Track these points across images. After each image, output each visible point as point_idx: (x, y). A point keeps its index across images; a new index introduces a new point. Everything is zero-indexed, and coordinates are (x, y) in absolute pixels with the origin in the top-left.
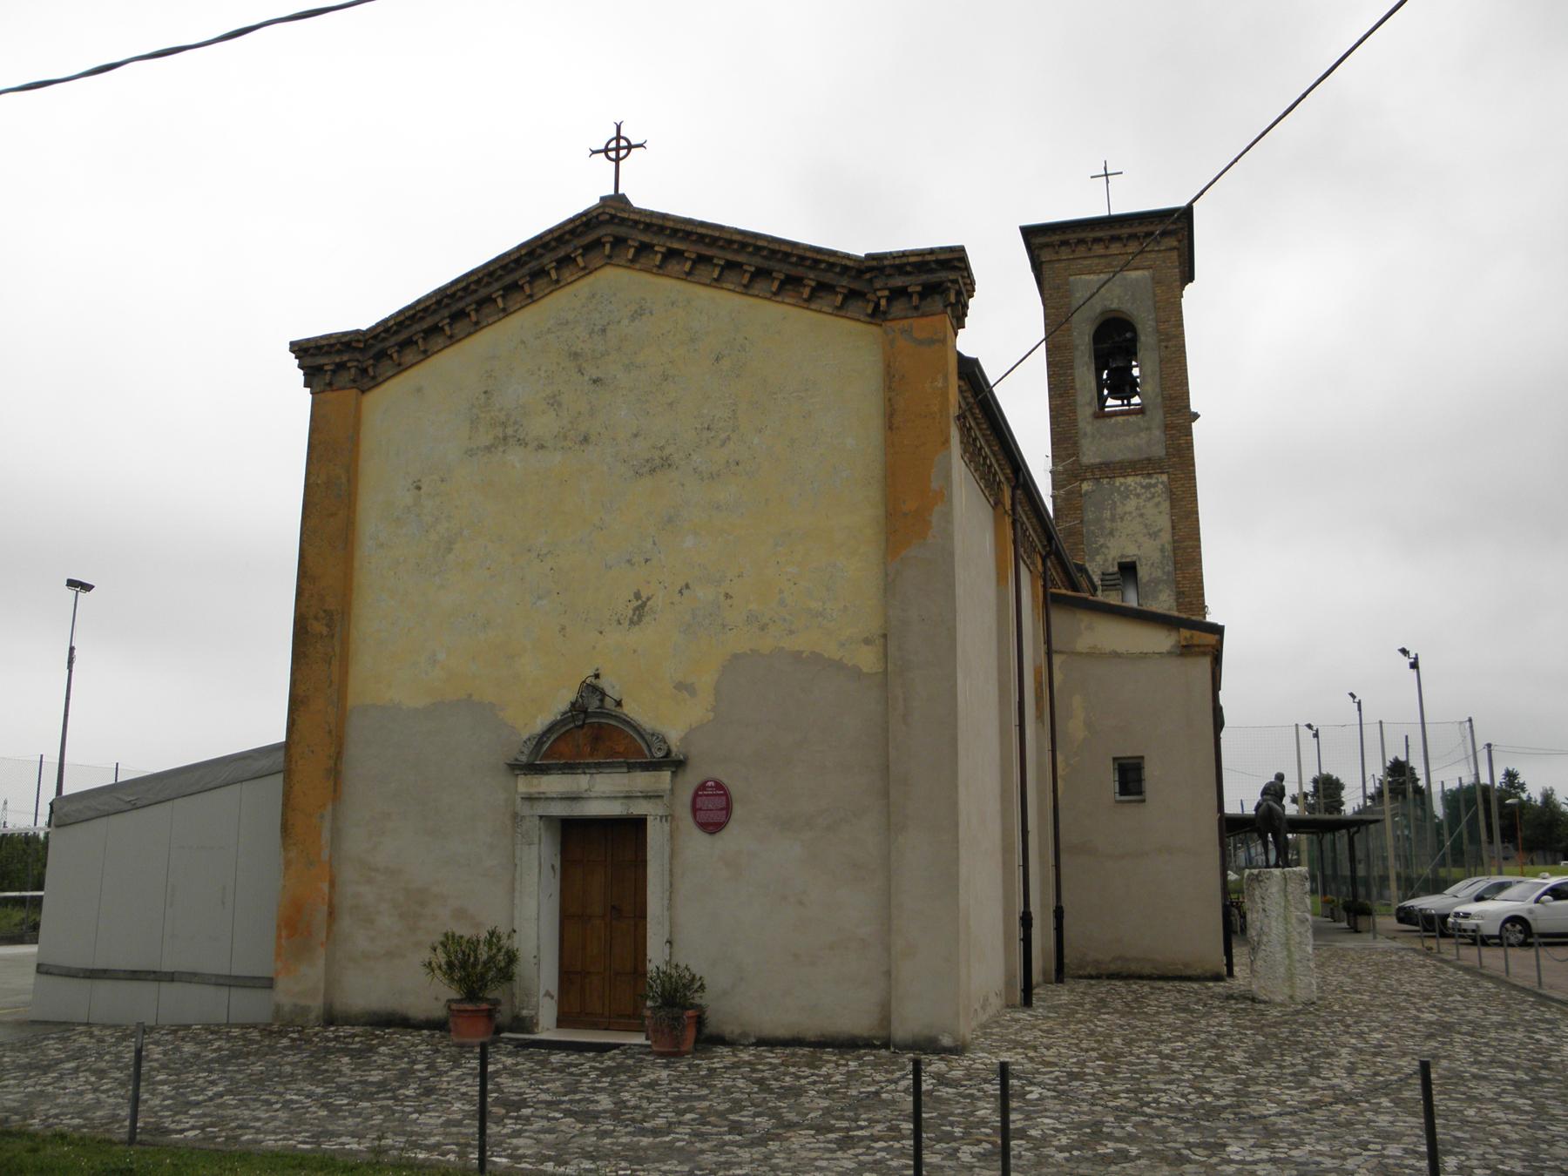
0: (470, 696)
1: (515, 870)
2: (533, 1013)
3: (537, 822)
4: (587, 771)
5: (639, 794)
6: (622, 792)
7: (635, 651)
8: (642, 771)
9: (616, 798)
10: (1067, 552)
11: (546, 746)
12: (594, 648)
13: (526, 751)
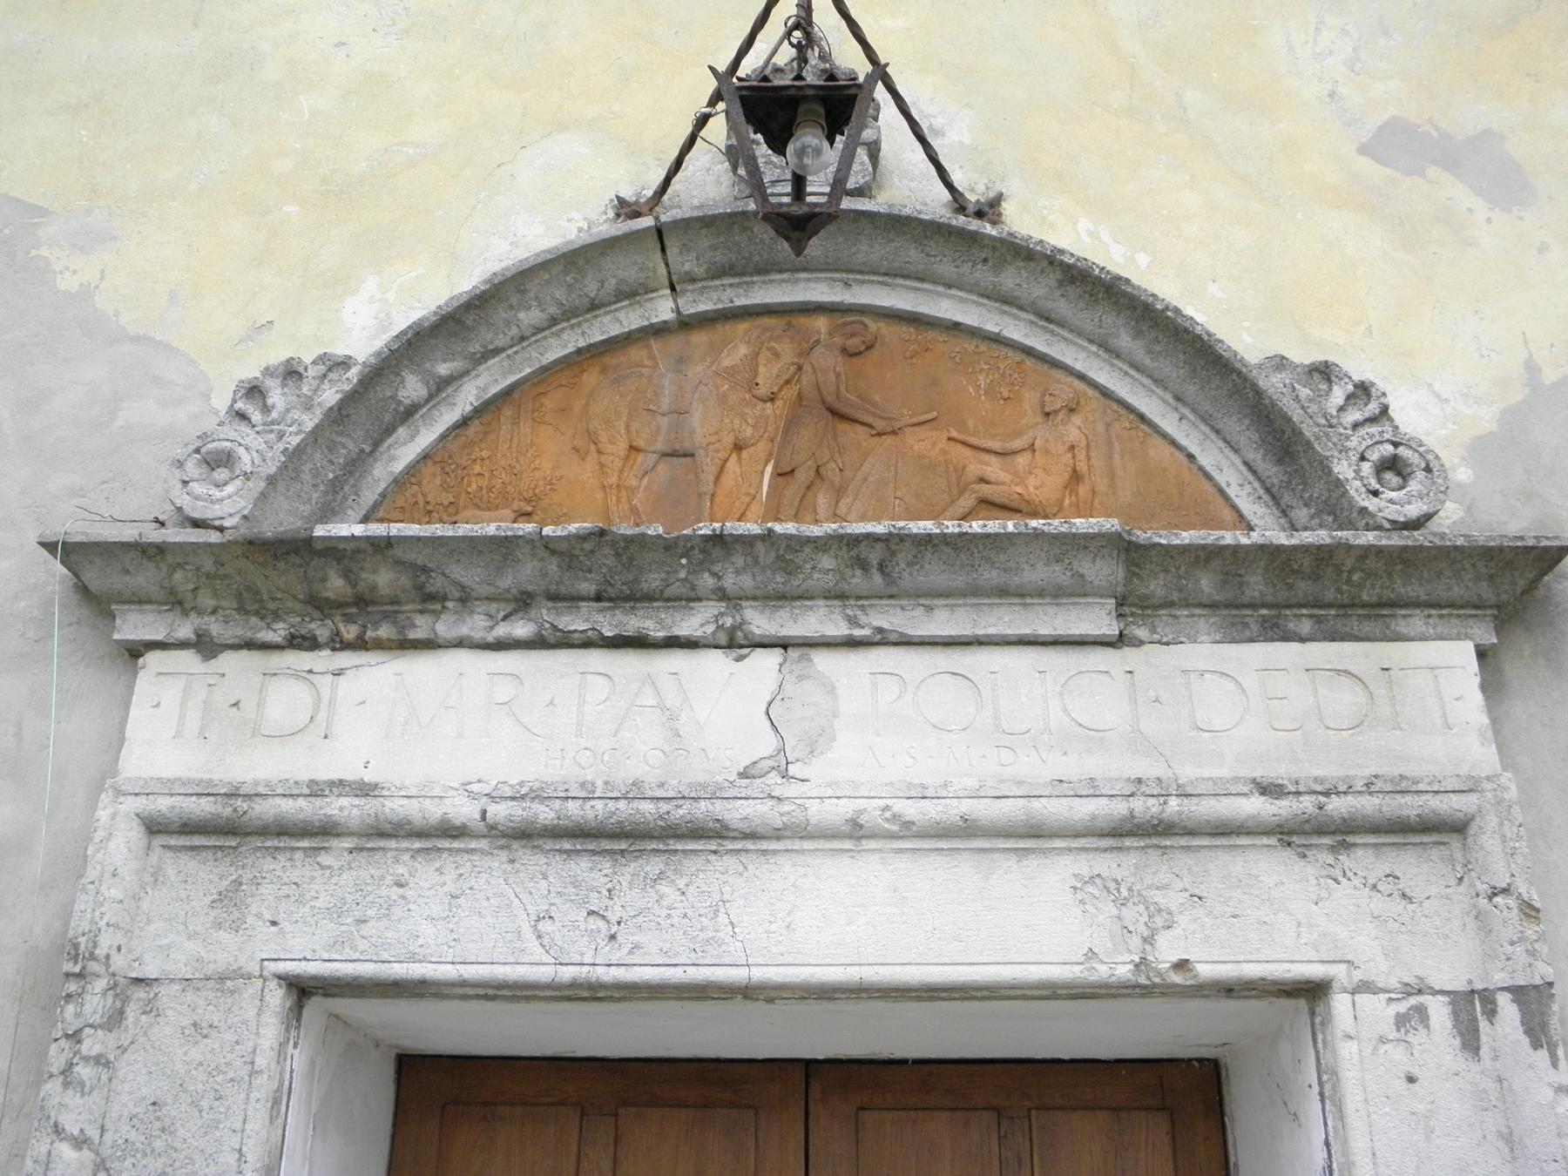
3: (271, 1030)
4: (761, 622)
5: (1255, 807)
6: (1092, 791)
8: (1236, 633)
10: (720, 306)
11: (406, 450)
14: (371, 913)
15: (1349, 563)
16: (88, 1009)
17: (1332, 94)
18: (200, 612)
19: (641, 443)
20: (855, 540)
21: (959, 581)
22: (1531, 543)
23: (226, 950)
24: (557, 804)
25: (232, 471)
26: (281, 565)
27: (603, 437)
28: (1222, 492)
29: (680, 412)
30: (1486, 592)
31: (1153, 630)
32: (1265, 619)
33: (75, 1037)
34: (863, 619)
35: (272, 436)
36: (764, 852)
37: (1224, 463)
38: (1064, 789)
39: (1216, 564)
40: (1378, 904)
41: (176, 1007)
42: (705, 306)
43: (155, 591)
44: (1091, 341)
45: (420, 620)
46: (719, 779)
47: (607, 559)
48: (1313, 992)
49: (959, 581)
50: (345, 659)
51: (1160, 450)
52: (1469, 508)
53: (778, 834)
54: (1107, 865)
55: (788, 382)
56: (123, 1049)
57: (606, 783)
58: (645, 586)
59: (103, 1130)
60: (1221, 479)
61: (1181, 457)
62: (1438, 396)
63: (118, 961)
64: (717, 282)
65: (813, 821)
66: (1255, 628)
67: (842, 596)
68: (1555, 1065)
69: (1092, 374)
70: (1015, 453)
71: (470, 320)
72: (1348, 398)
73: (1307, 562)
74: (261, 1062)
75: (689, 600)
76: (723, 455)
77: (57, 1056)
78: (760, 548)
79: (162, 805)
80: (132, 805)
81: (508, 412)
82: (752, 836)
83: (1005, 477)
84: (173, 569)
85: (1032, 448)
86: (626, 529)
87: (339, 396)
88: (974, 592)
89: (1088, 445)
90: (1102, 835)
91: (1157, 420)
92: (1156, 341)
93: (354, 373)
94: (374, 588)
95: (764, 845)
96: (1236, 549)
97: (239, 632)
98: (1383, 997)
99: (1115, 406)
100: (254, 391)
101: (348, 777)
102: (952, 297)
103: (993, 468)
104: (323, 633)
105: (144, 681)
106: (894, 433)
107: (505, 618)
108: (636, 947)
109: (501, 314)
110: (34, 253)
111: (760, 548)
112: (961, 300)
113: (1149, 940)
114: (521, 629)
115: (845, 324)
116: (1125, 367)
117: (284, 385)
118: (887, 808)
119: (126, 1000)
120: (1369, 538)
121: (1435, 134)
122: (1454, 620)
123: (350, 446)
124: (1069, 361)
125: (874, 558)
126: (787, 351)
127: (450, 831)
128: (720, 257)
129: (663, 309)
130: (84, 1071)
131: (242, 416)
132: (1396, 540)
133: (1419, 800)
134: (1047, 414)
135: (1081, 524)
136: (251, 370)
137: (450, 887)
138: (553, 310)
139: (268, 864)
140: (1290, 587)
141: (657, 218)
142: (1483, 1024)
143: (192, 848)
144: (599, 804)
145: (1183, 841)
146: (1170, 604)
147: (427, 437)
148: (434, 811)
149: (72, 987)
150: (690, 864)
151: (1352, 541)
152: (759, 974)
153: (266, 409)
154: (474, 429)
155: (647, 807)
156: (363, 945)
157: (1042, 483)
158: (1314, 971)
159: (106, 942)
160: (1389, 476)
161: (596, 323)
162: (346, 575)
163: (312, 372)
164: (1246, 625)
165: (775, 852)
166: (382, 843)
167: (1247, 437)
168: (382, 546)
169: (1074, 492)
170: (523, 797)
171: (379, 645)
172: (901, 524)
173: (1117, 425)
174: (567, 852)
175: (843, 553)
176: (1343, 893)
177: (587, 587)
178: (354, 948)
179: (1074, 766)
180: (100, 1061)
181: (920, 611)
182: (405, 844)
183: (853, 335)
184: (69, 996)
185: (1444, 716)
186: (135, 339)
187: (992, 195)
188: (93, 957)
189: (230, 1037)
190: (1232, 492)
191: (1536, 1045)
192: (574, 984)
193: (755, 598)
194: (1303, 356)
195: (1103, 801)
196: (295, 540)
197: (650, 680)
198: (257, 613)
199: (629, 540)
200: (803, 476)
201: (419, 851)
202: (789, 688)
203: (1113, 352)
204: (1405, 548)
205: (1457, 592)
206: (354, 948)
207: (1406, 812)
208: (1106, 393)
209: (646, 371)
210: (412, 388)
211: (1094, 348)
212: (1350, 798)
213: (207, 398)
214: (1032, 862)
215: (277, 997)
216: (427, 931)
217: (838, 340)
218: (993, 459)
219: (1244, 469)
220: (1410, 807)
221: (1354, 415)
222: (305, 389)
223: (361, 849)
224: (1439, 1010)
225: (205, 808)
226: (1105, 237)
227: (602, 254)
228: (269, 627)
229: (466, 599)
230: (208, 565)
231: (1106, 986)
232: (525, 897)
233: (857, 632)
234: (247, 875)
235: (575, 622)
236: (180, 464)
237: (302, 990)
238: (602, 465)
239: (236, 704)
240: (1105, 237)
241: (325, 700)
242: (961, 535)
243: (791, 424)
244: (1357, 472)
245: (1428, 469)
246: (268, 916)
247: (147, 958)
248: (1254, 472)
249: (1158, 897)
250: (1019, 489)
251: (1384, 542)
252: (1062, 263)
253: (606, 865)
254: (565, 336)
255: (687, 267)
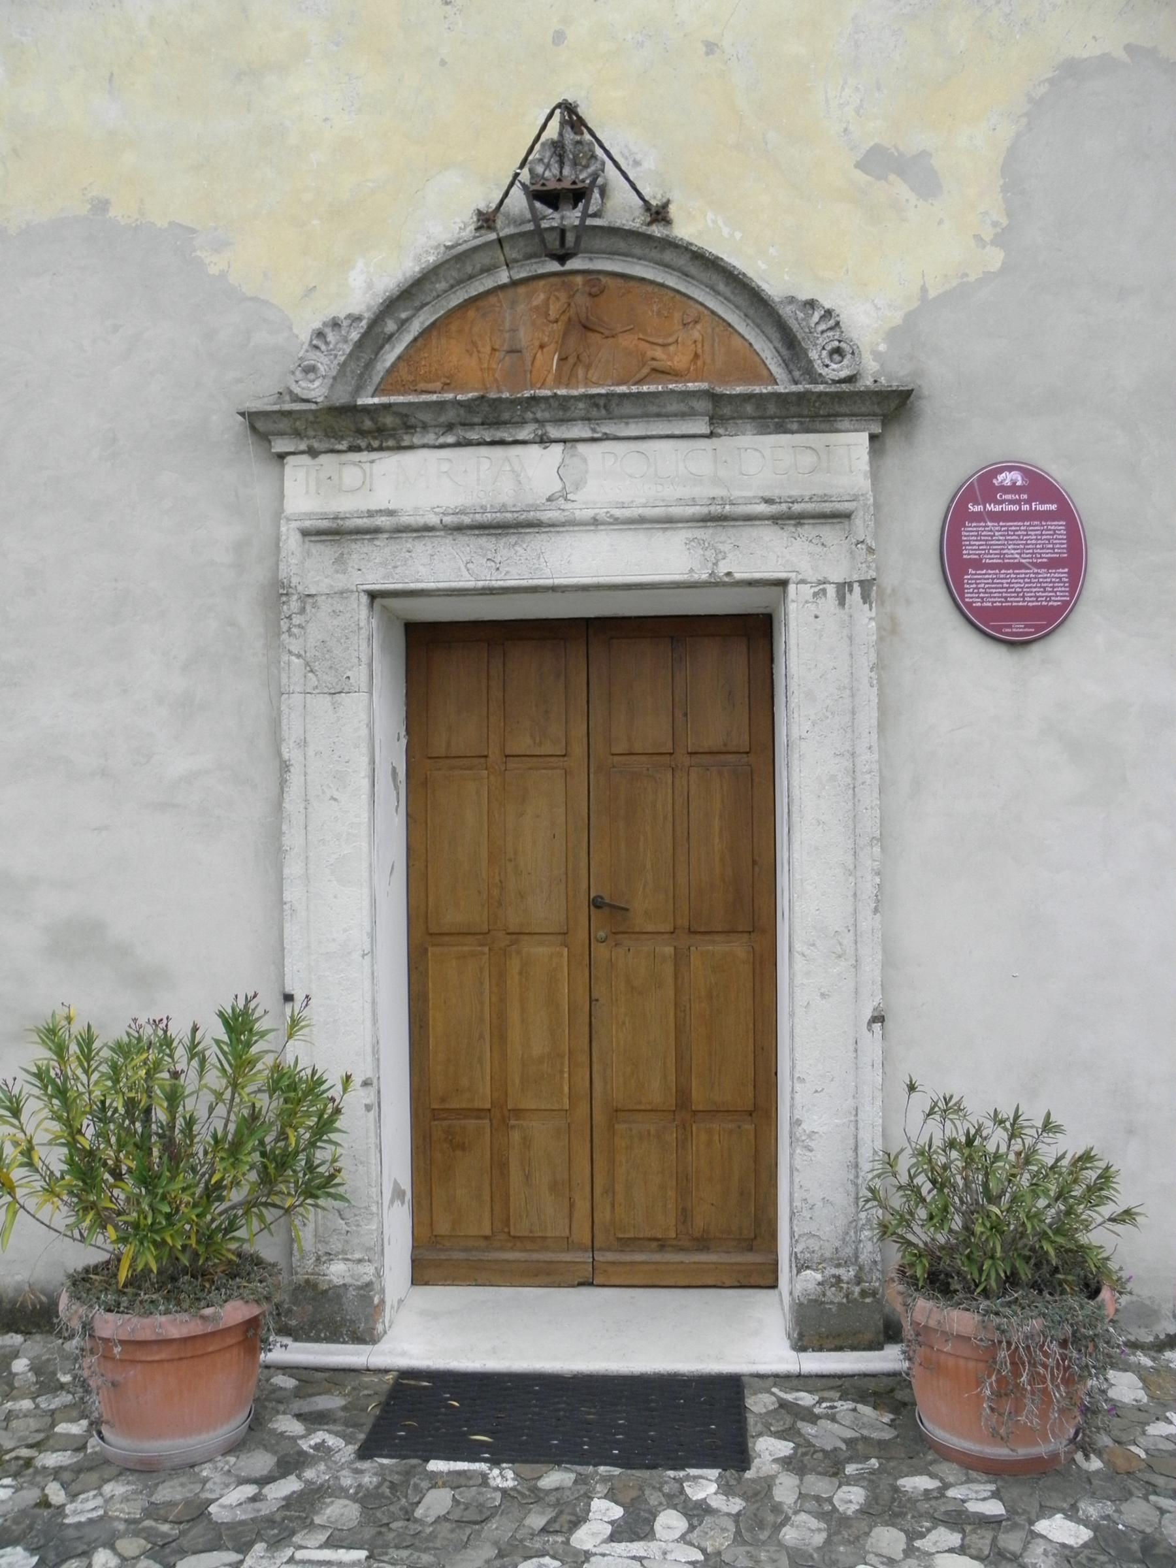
0: (101, 206)
1: (282, 783)
2: (367, 1272)
3: (364, 612)
4: (554, 432)
5: (762, 508)
6: (693, 502)
7: (711, 48)
8: (764, 430)
9: (668, 522)
10: (530, 274)
11: (390, 356)
12: (559, 37)
13: (325, 364)
14: (399, 563)
15: (813, 398)
16: (292, 607)
17: (846, 130)
18: (308, 438)
19: (497, 347)
20: (592, 396)
21: (639, 411)
22: (894, 388)
23: (341, 582)
24: (471, 515)
25: (316, 374)
26: (343, 416)
27: (480, 344)
28: (764, 362)
29: (514, 330)
30: (877, 409)
31: (726, 429)
32: (777, 423)
33: (289, 618)
34: (598, 429)
35: (332, 357)
36: (558, 532)
37: (766, 348)
38: (682, 502)
39: (753, 400)
40: (811, 548)
41: (325, 606)
42: (523, 275)
43: (288, 430)
44: (707, 286)
45: (407, 437)
46: (538, 502)
47: (485, 408)
48: (783, 584)
49: (639, 411)
50: (374, 455)
51: (736, 342)
52: (882, 365)
53: (563, 524)
54: (700, 533)
55: (564, 312)
56: (307, 622)
57: (491, 506)
58: (503, 419)
59: (305, 652)
60: (763, 355)
61: (747, 345)
62: (876, 306)
63: (300, 588)
64: (528, 262)
65: (577, 519)
66: (772, 427)
67: (589, 419)
68: (871, 610)
69: (707, 303)
70: (669, 344)
71: (414, 291)
72: (821, 318)
73: (794, 398)
74: (362, 624)
75: (522, 423)
76: (534, 351)
77: (284, 625)
78: (551, 400)
79: (307, 524)
80: (294, 525)
81: (435, 333)
82: (553, 525)
83: (664, 357)
84: (295, 420)
85: (677, 342)
86: (493, 395)
87: (359, 336)
88: (646, 416)
89: (703, 340)
90: (698, 521)
91: (736, 326)
92: (735, 288)
93: (364, 323)
94: (384, 425)
95: (558, 529)
96: (761, 395)
97: (327, 446)
98: (809, 585)
99: (717, 319)
100: (320, 334)
101: (383, 508)
102: (641, 264)
103: (658, 353)
104: (363, 444)
105: (288, 470)
106: (613, 336)
107: (443, 434)
108: (507, 572)
109: (428, 286)
110: (194, 254)
111: (551, 400)
112: (646, 266)
113: (715, 564)
114: (450, 439)
115: (590, 280)
116: (722, 299)
117: (333, 331)
118: (608, 512)
119: (305, 603)
120: (821, 388)
121: (896, 154)
122: (863, 422)
123: (366, 356)
124: (696, 296)
125: (602, 402)
126: (563, 296)
127: (428, 528)
128: (529, 250)
129: (503, 277)
130: (295, 630)
131: (317, 347)
132: (833, 389)
133: (831, 505)
134: (685, 325)
135: (691, 386)
136: (317, 325)
137: (430, 552)
138: (452, 281)
139: (353, 546)
140: (788, 410)
141: (498, 234)
142: (848, 595)
143: (321, 541)
144: (489, 515)
145: (732, 523)
146: (734, 418)
147: (399, 349)
148: (421, 521)
149: (284, 599)
150: (528, 538)
151: (814, 390)
152: (557, 581)
153: (327, 343)
154: (420, 341)
155: (509, 515)
156: (397, 576)
157: (680, 360)
158: (782, 575)
159: (294, 581)
160: (836, 357)
161: (472, 286)
162: (372, 419)
163: (345, 323)
164: (768, 426)
165: (562, 532)
166: (400, 535)
167: (776, 336)
168: (387, 407)
169: (695, 364)
170: (457, 513)
171: (389, 449)
172: (612, 388)
173: (717, 329)
174: (477, 535)
175: (588, 401)
176: (798, 544)
177: (477, 420)
178: (393, 578)
179: (686, 492)
180: (300, 626)
181: (623, 425)
182: (409, 535)
183: (594, 286)
184: (284, 603)
185: (850, 467)
186: (252, 299)
187: (664, 200)
188: (290, 587)
189: (348, 615)
190: (767, 362)
191: (865, 603)
192: (483, 589)
193: (550, 421)
194: (804, 296)
195: (698, 507)
196: (349, 406)
197: (507, 459)
198: (333, 437)
199: (495, 400)
200: (571, 360)
201: (416, 537)
202: (567, 461)
203: (717, 293)
204: (837, 392)
205: (863, 410)
206: (393, 578)
207: (825, 510)
208: (713, 312)
209: (497, 309)
210: (390, 326)
211: (708, 290)
212: (802, 504)
213: (291, 329)
214: (669, 533)
215: (364, 599)
216: (422, 570)
217: (587, 289)
218: (658, 348)
219: (774, 350)
220: (827, 507)
221: (823, 327)
222: (343, 332)
223: (391, 538)
224: (831, 590)
225: (324, 524)
226: (720, 223)
227: (474, 253)
228: (339, 443)
229: (425, 427)
230: (311, 418)
231: (697, 582)
232: (461, 554)
233: (596, 435)
234: (346, 551)
235: (473, 435)
236: (293, 373)
237: (373, 596)
238: (480, 359)
239: (330, 478)
240: (720, 223)
241: (368, 475)
242: (638, 393)
243: (566, 334)
244: (820, 356)
245: (853, 353)
246: (357, 567)
247: (310, 586)
248: (778, 352)
249: (721, 547)
250: (669, 363)
251: (828, 390)
252: (691, 250)
253: (493, 540)
254: (458, 293)
255: (514, 256)
